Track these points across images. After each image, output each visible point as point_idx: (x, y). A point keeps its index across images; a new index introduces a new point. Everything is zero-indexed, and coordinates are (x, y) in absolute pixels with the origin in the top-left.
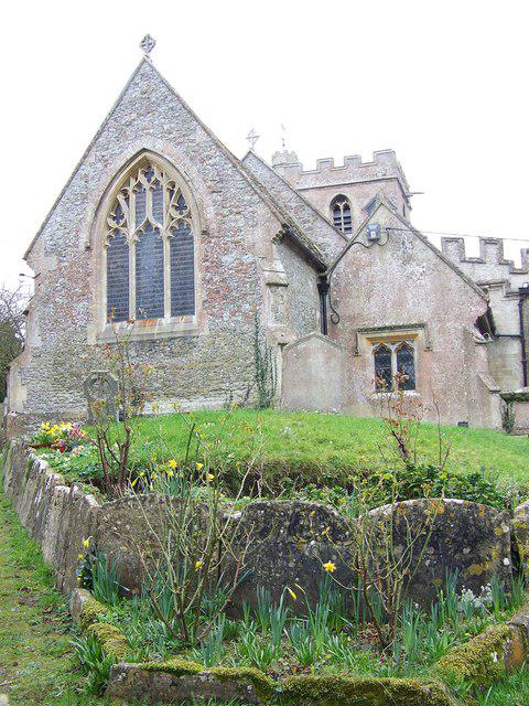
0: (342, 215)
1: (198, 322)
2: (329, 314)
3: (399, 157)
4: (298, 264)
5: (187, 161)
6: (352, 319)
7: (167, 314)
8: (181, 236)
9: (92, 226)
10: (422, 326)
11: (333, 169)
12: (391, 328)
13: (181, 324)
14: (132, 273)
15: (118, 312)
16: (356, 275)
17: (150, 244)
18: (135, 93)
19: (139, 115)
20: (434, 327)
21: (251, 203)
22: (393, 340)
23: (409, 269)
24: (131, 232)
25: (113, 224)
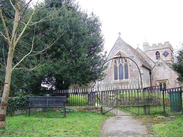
0: (158, 55)
1: (129, 80)
2: (151, 78)
3: (170, 43)
4: (145, 70)
5: (127, 54)
6: (155, 79)
7: (124, 78)
8: (126, 66)
9: (112, 64)
10: (167, 80)
11: (156, 46)
12: (162, 80)
13: (126, 80)
14: (118, 72)
15: (116, 78)
16: (156, 71)
17: (121, 67)
18: (118, 42)
19: (119, 46)
20: (170, 80)
21: (137, 61)
22: (162, 82)
23: (165, 70)
24: (118, 65)
25: (115, 64)
